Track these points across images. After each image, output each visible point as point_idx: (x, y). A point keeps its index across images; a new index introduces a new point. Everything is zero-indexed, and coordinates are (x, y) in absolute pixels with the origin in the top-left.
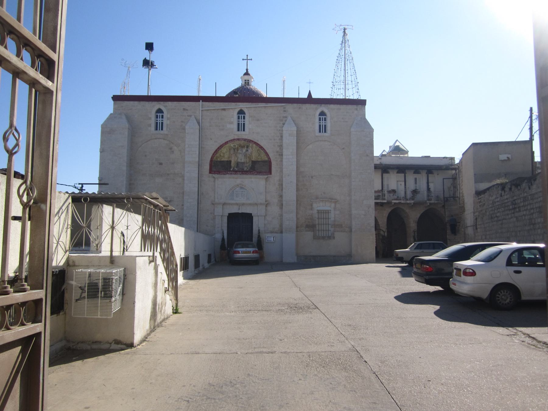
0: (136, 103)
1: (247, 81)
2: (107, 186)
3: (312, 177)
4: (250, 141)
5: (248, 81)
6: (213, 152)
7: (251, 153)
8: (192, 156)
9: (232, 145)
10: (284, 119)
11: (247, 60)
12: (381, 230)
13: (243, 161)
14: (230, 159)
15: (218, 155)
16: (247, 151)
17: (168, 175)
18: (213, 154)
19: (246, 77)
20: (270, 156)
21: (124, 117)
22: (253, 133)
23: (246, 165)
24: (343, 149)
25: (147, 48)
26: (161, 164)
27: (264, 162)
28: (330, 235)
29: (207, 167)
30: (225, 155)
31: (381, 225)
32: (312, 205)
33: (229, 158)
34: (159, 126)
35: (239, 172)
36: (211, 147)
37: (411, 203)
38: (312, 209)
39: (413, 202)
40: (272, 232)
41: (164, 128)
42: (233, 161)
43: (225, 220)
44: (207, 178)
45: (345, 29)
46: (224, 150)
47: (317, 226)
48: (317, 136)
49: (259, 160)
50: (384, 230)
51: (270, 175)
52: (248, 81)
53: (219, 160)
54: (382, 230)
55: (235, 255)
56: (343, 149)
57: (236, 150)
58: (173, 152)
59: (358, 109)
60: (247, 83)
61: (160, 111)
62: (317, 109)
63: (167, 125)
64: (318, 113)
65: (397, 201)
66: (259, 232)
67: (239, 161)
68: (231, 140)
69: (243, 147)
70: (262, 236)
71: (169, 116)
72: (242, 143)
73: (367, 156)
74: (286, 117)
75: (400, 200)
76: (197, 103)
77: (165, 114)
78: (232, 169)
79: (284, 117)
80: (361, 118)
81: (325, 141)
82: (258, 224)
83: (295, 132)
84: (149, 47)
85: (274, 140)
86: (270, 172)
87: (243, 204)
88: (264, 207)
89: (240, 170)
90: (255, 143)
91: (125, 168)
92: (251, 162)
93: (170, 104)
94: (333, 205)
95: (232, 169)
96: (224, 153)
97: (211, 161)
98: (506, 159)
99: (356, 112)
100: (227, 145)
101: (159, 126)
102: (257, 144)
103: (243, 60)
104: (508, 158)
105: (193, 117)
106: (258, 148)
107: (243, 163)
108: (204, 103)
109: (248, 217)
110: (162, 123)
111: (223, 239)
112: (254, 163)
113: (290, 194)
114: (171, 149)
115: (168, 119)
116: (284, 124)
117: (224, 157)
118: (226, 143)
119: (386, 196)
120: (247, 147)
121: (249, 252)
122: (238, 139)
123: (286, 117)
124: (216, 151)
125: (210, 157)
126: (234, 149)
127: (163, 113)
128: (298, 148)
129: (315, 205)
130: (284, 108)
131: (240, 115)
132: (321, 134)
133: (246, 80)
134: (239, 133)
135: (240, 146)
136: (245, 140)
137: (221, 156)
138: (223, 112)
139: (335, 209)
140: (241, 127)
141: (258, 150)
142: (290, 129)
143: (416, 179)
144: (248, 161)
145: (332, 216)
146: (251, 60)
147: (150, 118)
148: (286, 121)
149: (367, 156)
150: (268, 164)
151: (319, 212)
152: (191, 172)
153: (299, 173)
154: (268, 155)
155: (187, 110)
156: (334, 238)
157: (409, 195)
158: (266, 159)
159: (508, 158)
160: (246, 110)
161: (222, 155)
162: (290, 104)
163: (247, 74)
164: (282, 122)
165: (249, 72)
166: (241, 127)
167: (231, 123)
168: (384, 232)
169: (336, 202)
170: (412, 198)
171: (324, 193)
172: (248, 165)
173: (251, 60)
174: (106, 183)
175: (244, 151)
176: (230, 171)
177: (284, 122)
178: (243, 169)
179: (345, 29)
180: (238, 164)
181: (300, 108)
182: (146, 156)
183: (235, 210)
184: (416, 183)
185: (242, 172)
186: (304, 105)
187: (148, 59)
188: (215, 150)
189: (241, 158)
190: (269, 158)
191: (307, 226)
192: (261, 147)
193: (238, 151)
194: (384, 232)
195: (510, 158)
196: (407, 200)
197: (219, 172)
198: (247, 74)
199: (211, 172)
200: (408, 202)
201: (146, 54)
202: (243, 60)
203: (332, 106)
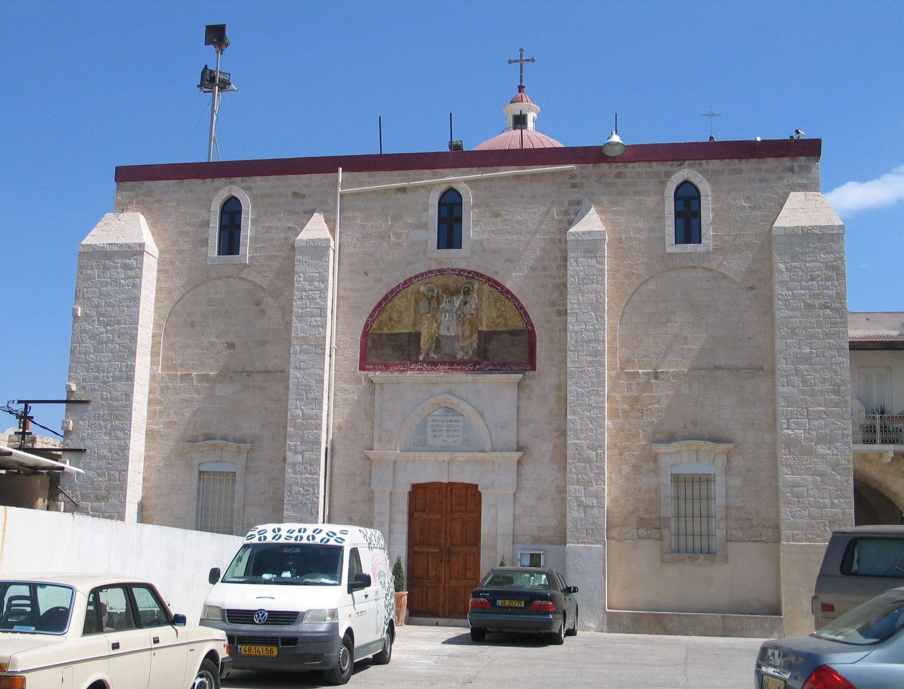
7: (477, 310)
9: (423, 289)
11: (521, 61)
13: (452, 333)
14: (417, 328)
15: (384, 317)
16: (466, 303)
24: (752, 288)
35: (443, 363)
42: (426, 331)
46: (400, 303)
51: (531, 373)
53: (386, 331)
59: (796, 168)
67: (443, 332)
69: (451, 292)
72: (451, 281)
86: (530, 363)
90: (489, 280)
95: (421, 358)
100: (409, 289)
103: (510, 62)
112: (486, 337)
118: (408, 283)
120: (467, 293)
126: (430, 300)
135: (444, 291)
136: (460, 272)
138: (401, 196)
139: (727, 470)
144: (467, 333)
145: (719, 490)
150: (528, 337)
154: (526, 314)
155: (303, 196)
158: (521, 325)
175: (457, 304)
176: (417, 362)
193: (439, 304)
201: (209, 56)
202: (510, 62)
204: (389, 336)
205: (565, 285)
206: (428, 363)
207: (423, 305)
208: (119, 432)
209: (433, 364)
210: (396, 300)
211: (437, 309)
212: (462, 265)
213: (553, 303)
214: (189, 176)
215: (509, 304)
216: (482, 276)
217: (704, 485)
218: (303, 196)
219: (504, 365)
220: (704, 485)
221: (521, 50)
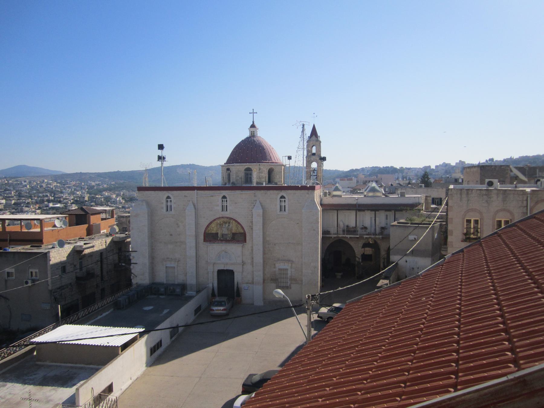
0: (152, 192)
1: (253, 133)
2: (137, 253)
3: (275, 245)
4: (231, 219)
5: (254, 132)
6: (205, 227)
7: (232, 227)
8: (191, 231)
9: (219, 222)
10: (255, 202)
11: (253, 113)
12: (357, 257)
13: (226, 233)
14: (217, 232)
15: (209, 229)
16: (229, 226)
17: (176, 243)
18: (206, 228)
19: (253, 129)
20: (245, 230)
21: (144, 204)
22: (233, 212)
23: (228, 236)
24: (298, 224)
25: (162, 145)
26: (171, 235)
27: (241, 233)
28: (288, 285)
29: (202, 237)
30: (214, 229)
31: (356, 253)
32: (275, 265)
33: (217, 231)
34: (168, 208)
35: (224, 241)
36: (204, 223)
37: (380, 238)
38: (275, 267)
39: (381, 236)
40: (247, 283)
41: (173, 210)
42: (220, 233)
43: (216, 274)
44: (203, 246)
45: (303, 125)
46: (213, 225)
47: (279, 279)
48: (279, 215)
49: (238, 232)
50: (359, 257)
51: (245, 243)
52: (254, 132)
53: (210, 232)
54: (358, 257)
55: (211, 311)
56: (298, 224)
57: (221, 225)
58: (179, 226)
59: (309, 193)
60: (253, 135)
61: (168, 197)
62: (278, 194)
63: (174, 207)
64: (279, 197)
65: (368, 236)
66: (238, 283)
67: (224, 233)
68: (218, 218)
69: (225, 223)
70: (239, 286)
71: (175, 201)
72: (225, 220)
73: (314, 230)
74: (256, 201)
75: (371, 235)
76: (193, 191)
77: (172, 199)
78: (219, 239)
79: (254, 201)
80: (311, 200)
81: (284, 218)
82: (238, 278)
83: (261, 213)
84: (161, 147)
85: (248, 217)
86: (245, 241)
87: (227, 264)
88: (241, 266)
89: (225, 240)
90: (234, 220)
91: (147, 241)
92: (231, 234)
93: (175, 192)
94: (290, 265)
95: (219, 239)
96: (213, 228)
97: (205, 233)
98: (414, 239)
99: (307, 196)
100: (215, 222)
101: (168, 208)
102: (236, 221)
103: (250, 113)
104: (415, 238)
105: (191, 202)
106: (236, 224)
107: (226, 235)
108: (198, 191)
109: (231, 272)
110: (171, 206)
111: (213, 289)
112: (234, 234)
113: (259, 258)
114: (177, 224)
115: (175, 203)
116: (254, 206)
117: (213, 230)
118: (215, 220)
119: (359, 232)
120: (229, 223)
121: (220, 310)
122: (223, 217)
123: (256, 201)
124: (208, 226)
125: (204, 230)
126: (220, 225)
127: (171, 199)
128: (264, 224)
129: (277, 265)
130: (255, 194)
131: (224, 199)
132: (282, 213)
133: (252, 132)
134: (223, 213)
135: (224, 223)
136: (227, 218)
137: (211, 229)
138: (212, 197)
139: (291, 268)
140: (224, 208)
141: (237, 225)
142: (258, 211)
143: (387, 216)
144: (230, 233)
145: (289, 272)
146: (257, 113)
147: (163, 203)
148: (256, 203)
149: (314, 230)
150: (244, 235)
151: (280, 269)
152: (191, 242)
153: (265, 241)
154: (244, 229)
155: (187, 197)
156: (291, 288)
157: (378, 230)
158: (242, 231)
159: (415, 238)
160: (227, 196)
161: (212, 228)
162: (259, 191)
163: (253, 126)
164: (253, 205)
165: (255, 124)
166: (224, 208)
167: (218, 206)
168: (359, 259)
169: (292, 262)
170: (381, 233)
171: (284, 256)
172: (230, 236)
173: (257, 113)
174: (136, 250)
175: (227, 226)
176: (218, 240)
177: (254, 204)
178: (226, 239)
179: (303, 125)
180: (223, 235)
181: (266, 193)
182: (161, 229)
183: (222, 267)
184: (387, 218)
185: (226, 241)
186: (269, 191)
187: (160, 155)
188: (207, 225)
189: (225, 231)
190: (244, 231)
191: (272, 280)
192: (239, 223)
193: (222, 226)
194: (359, 259)
195: (416, 238)
196: (376, 235)
197: (210, 241)
198: (253, 126)
199: (205, 240)
200: (377, 237)
201: (160, 153)
202: (250, 113)
203: (290, 191)
204: (210, 233)
205: (253, 221)
206: (220, 240)
207: (219, 226)
208: (104, 193)
209: (222, 241)
210: (212, 225)
211: (222, 227)
212: (228, 216)
213: (250, 226)
214: (157, 190)
215: (240, 226)
216: (233, 219)
217: (286, 271)
218: (187, 197)
219: (238, 241)
220: (286, 271)
221: (253, 110)
